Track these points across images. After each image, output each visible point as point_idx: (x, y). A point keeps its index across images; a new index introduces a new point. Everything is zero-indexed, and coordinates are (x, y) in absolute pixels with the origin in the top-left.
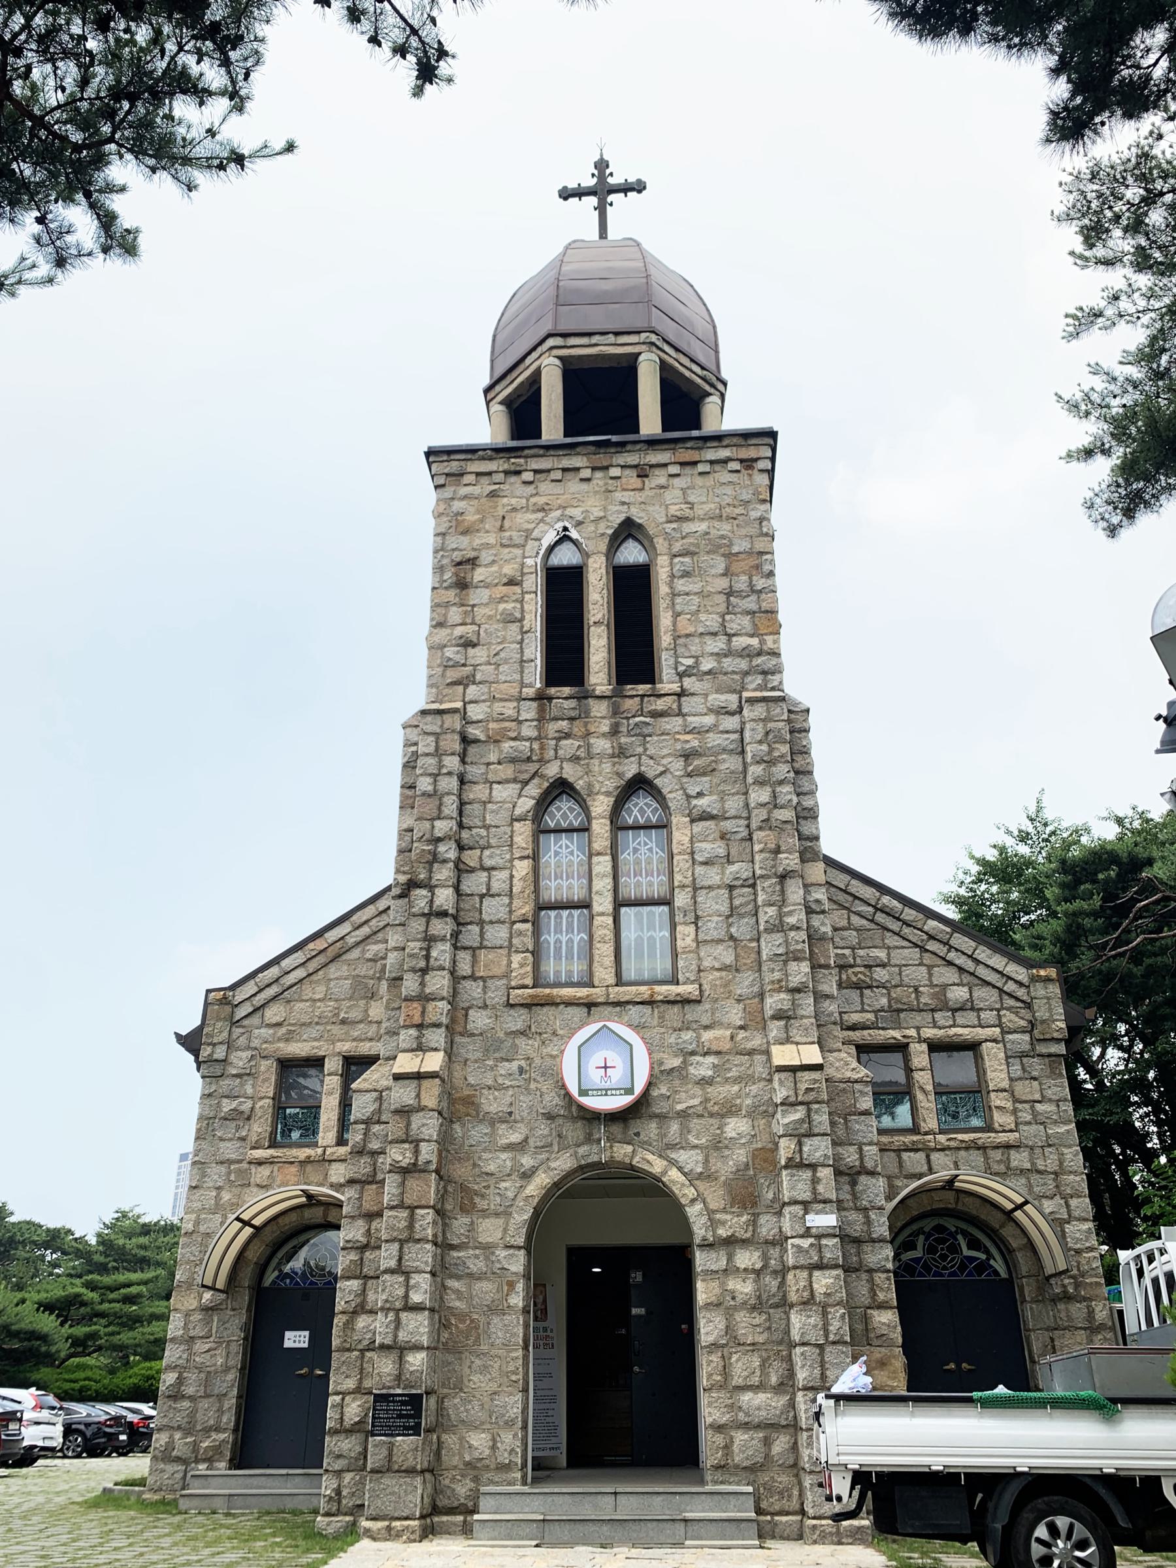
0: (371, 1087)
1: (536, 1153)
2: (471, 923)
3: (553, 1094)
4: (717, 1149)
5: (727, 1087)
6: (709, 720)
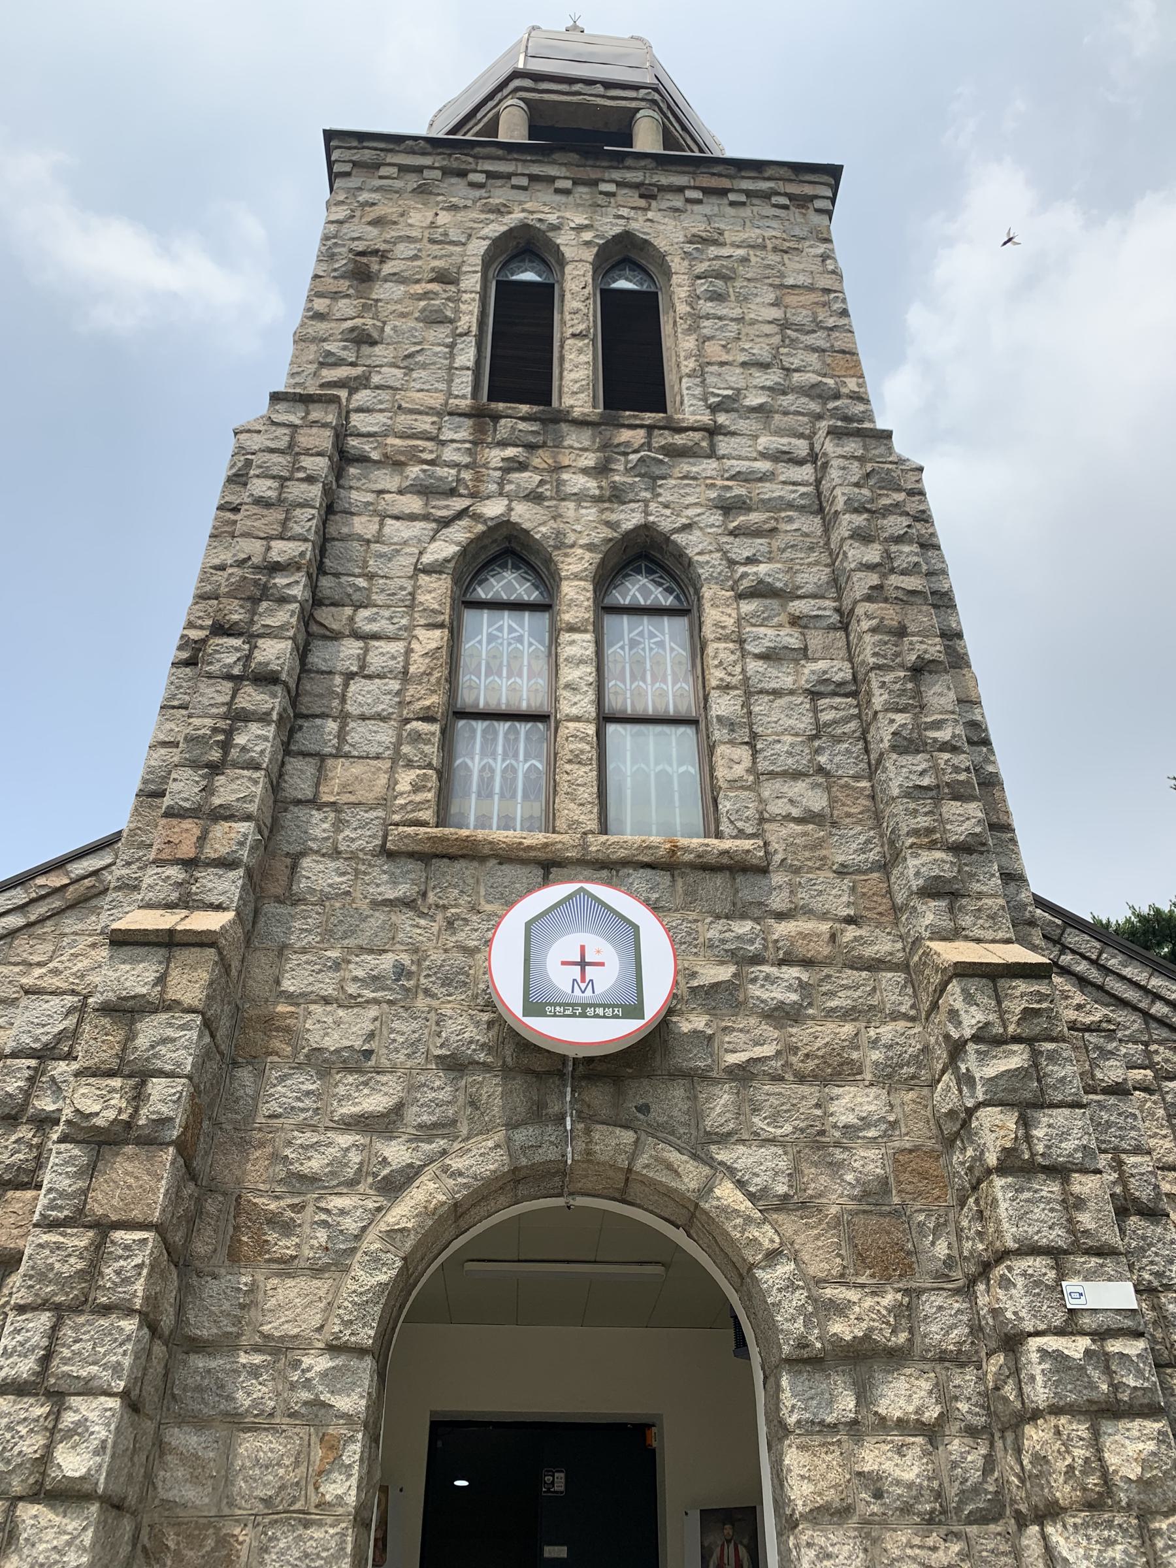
0: (64, 986)
1: (417, 1139)
2: (323, 716)
3: (464, 1020)
4: (819, 1146)
5: (830, 1026)
6: (764, 466)
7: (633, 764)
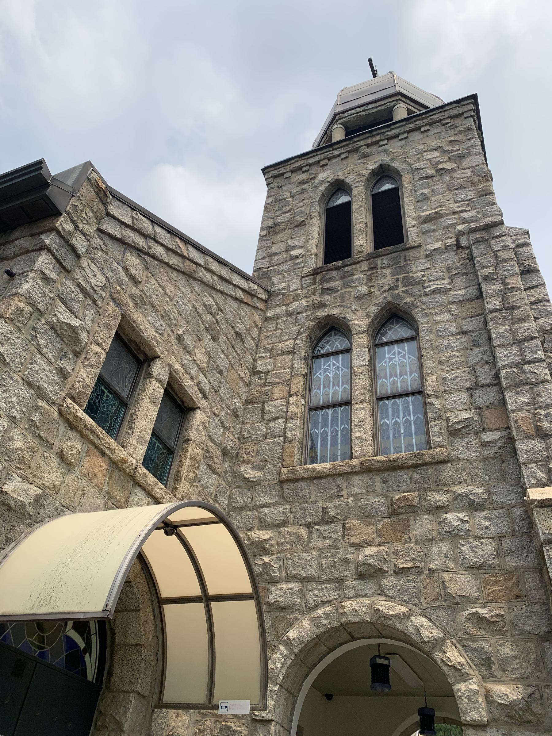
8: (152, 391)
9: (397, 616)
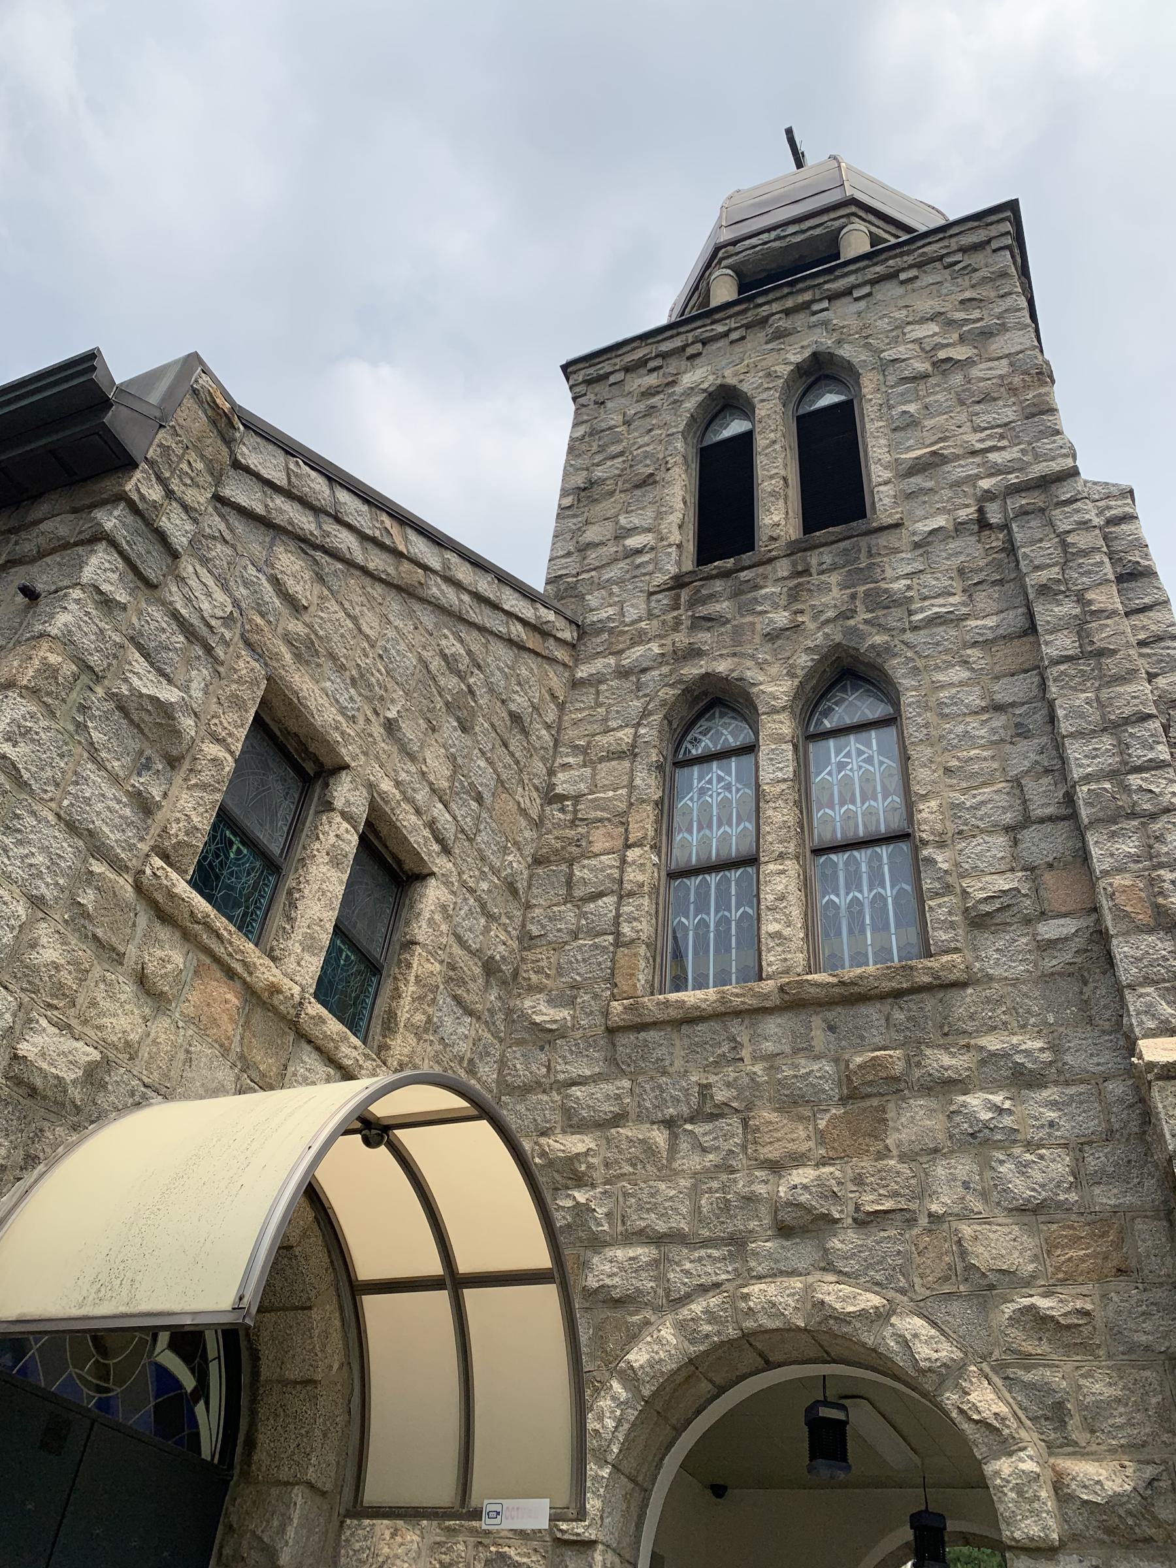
7: (717, 912)
8: (332, 839)
9: (862, 1314)
